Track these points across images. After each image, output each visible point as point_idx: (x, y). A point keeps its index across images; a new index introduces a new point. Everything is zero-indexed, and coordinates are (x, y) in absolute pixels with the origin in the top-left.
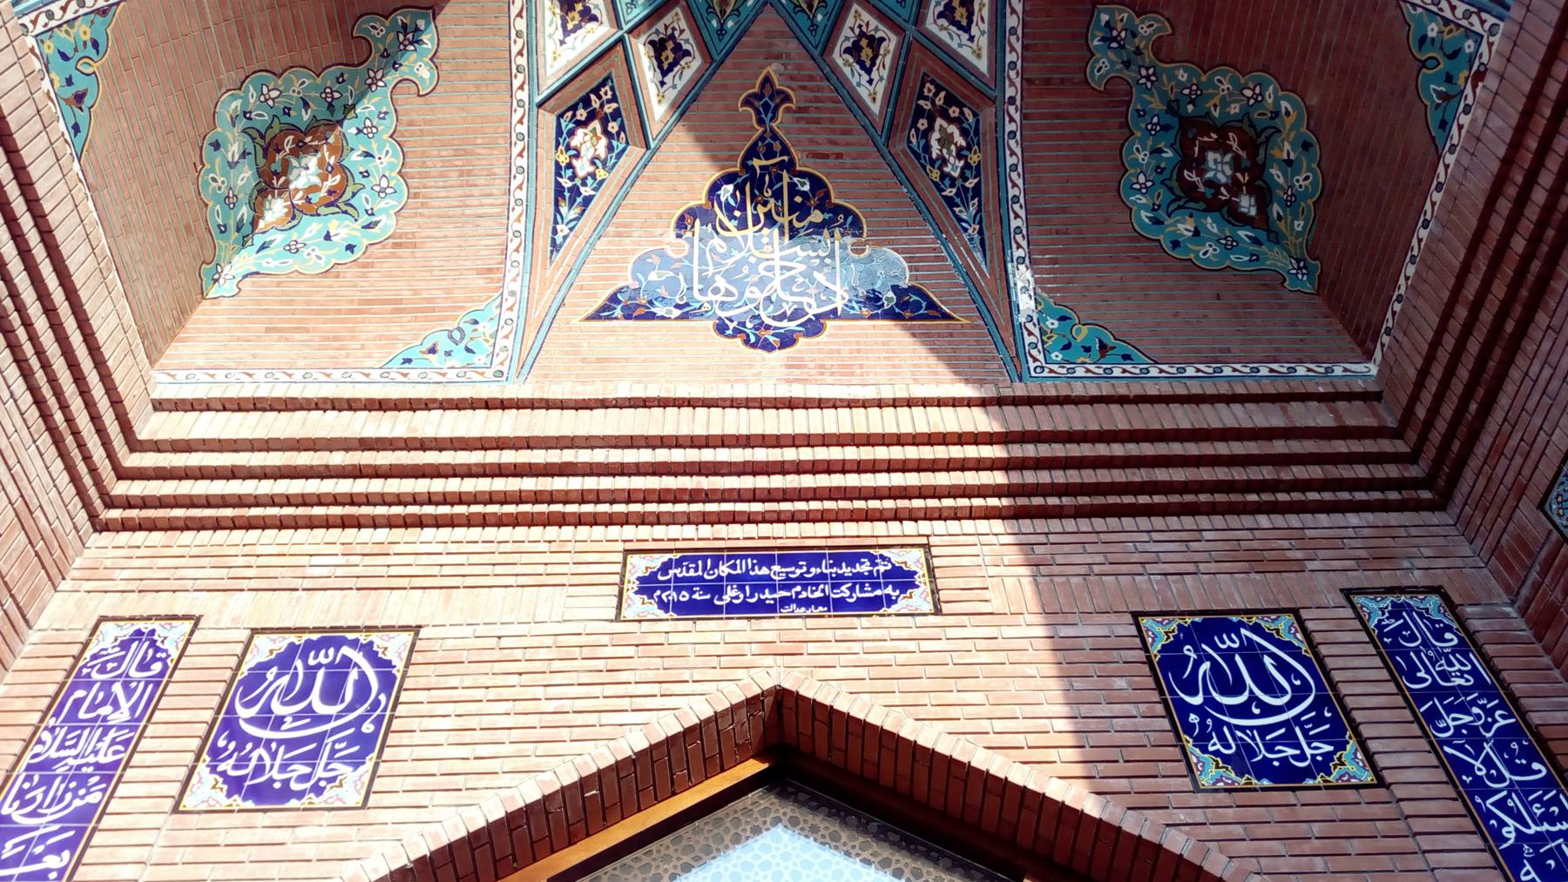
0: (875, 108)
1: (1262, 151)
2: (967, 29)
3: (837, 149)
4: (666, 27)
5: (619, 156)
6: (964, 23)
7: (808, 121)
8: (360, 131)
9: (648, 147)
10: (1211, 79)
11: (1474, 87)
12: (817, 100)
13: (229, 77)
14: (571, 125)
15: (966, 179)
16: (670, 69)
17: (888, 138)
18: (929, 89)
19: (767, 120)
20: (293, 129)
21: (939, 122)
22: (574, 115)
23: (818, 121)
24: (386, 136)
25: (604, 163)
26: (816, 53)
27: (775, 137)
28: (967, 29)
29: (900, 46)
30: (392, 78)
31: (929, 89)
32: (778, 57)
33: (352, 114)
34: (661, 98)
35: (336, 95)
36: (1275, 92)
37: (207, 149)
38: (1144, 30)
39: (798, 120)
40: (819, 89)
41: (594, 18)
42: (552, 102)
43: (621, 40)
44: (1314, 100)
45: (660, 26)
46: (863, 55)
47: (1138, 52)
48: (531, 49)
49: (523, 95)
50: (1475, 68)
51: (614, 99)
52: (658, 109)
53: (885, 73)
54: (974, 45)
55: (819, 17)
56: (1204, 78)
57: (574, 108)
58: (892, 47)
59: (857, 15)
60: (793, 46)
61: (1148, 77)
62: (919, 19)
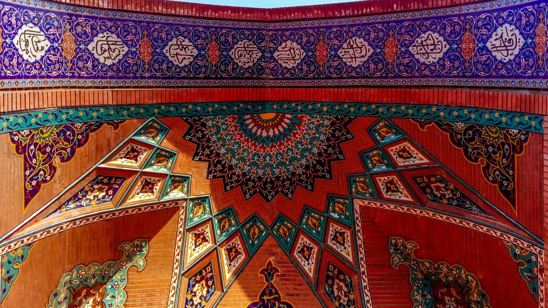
0: (311, 275)
1: (466, 297)
2: (343, 245)
3: (297, 292)
4: (233, 243)
5: (211, 296)
6: (342, 242)
7: (286, 280)
8: (112, 287)
9: (223, 291)
10: (439, 266)
11: (542, 275)
12: (289, 271)
13: (67, 267)
14: (194, 283)
15: (456, 195)
16: (233, 259)
17: (317, 288)
18: (331, 268)
19: (269, 280)
20: (87, 287)
21: (336, 281)
22: (195, 278)
23: (289, 280)
24: (122, 289)
25: (205, 298)
26: (288, 253)
27: (273, 287)
28: (343, 245)
29: (319, 250)
30: (129, 265)
31: (331, 268)
32: (273, 254)
33: (111, 280)
34: (229, 270)
35: (107, 272)
36: (465, 272)
37: (52, 296)
38: (409, 246)
39: (282, 279)
40: (290, 267)
41: (207, 241)
42: (188, 273)
43: (216, 248)
44: (481, 277)
45: (230, 243)
46: (305, 253)
47: (408, 255)
48: (182, 253)
49: (177, 271)
50: (539, 268)
51: (211, 272)
52: (228, 276)
53: (314, 261)
54: (346, 251)
55: (289, 240)
56: (436, 266)
57: (196, 275)
58: (316, 251)
59: (392, 150)
60: (279, 250)
61: (414, 265)
62: (325, 241)
